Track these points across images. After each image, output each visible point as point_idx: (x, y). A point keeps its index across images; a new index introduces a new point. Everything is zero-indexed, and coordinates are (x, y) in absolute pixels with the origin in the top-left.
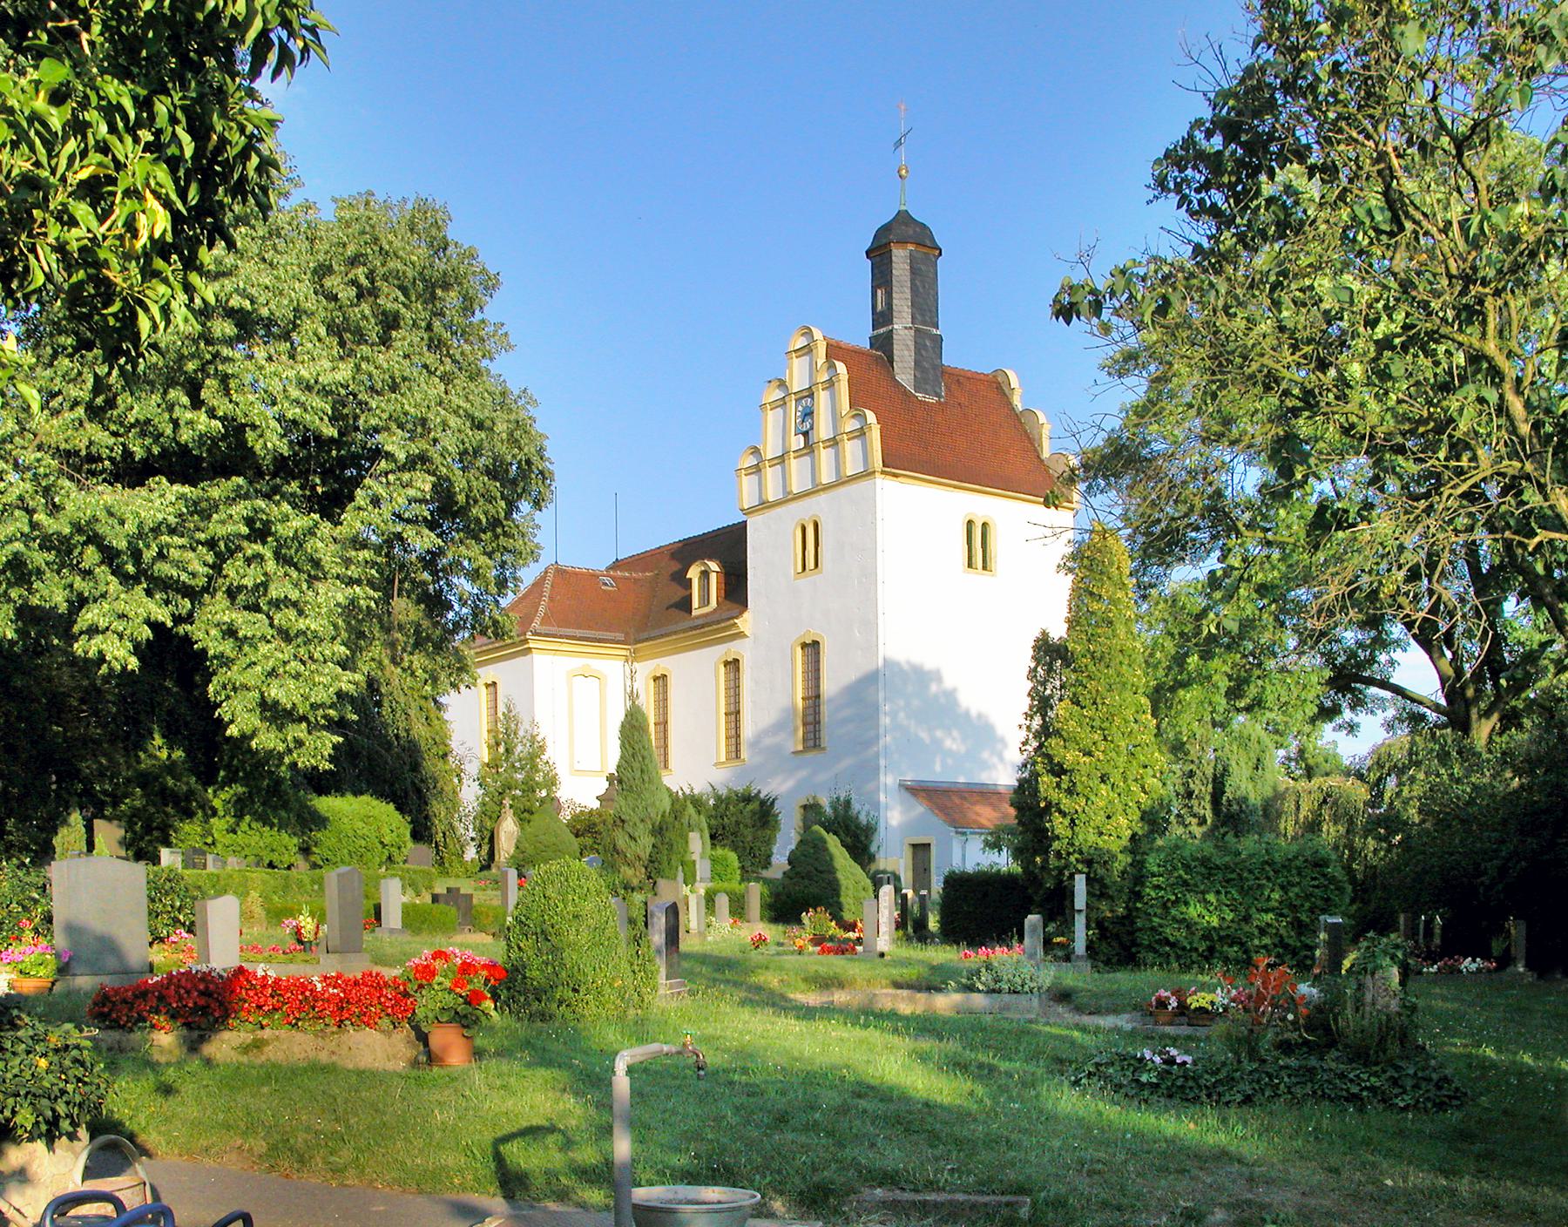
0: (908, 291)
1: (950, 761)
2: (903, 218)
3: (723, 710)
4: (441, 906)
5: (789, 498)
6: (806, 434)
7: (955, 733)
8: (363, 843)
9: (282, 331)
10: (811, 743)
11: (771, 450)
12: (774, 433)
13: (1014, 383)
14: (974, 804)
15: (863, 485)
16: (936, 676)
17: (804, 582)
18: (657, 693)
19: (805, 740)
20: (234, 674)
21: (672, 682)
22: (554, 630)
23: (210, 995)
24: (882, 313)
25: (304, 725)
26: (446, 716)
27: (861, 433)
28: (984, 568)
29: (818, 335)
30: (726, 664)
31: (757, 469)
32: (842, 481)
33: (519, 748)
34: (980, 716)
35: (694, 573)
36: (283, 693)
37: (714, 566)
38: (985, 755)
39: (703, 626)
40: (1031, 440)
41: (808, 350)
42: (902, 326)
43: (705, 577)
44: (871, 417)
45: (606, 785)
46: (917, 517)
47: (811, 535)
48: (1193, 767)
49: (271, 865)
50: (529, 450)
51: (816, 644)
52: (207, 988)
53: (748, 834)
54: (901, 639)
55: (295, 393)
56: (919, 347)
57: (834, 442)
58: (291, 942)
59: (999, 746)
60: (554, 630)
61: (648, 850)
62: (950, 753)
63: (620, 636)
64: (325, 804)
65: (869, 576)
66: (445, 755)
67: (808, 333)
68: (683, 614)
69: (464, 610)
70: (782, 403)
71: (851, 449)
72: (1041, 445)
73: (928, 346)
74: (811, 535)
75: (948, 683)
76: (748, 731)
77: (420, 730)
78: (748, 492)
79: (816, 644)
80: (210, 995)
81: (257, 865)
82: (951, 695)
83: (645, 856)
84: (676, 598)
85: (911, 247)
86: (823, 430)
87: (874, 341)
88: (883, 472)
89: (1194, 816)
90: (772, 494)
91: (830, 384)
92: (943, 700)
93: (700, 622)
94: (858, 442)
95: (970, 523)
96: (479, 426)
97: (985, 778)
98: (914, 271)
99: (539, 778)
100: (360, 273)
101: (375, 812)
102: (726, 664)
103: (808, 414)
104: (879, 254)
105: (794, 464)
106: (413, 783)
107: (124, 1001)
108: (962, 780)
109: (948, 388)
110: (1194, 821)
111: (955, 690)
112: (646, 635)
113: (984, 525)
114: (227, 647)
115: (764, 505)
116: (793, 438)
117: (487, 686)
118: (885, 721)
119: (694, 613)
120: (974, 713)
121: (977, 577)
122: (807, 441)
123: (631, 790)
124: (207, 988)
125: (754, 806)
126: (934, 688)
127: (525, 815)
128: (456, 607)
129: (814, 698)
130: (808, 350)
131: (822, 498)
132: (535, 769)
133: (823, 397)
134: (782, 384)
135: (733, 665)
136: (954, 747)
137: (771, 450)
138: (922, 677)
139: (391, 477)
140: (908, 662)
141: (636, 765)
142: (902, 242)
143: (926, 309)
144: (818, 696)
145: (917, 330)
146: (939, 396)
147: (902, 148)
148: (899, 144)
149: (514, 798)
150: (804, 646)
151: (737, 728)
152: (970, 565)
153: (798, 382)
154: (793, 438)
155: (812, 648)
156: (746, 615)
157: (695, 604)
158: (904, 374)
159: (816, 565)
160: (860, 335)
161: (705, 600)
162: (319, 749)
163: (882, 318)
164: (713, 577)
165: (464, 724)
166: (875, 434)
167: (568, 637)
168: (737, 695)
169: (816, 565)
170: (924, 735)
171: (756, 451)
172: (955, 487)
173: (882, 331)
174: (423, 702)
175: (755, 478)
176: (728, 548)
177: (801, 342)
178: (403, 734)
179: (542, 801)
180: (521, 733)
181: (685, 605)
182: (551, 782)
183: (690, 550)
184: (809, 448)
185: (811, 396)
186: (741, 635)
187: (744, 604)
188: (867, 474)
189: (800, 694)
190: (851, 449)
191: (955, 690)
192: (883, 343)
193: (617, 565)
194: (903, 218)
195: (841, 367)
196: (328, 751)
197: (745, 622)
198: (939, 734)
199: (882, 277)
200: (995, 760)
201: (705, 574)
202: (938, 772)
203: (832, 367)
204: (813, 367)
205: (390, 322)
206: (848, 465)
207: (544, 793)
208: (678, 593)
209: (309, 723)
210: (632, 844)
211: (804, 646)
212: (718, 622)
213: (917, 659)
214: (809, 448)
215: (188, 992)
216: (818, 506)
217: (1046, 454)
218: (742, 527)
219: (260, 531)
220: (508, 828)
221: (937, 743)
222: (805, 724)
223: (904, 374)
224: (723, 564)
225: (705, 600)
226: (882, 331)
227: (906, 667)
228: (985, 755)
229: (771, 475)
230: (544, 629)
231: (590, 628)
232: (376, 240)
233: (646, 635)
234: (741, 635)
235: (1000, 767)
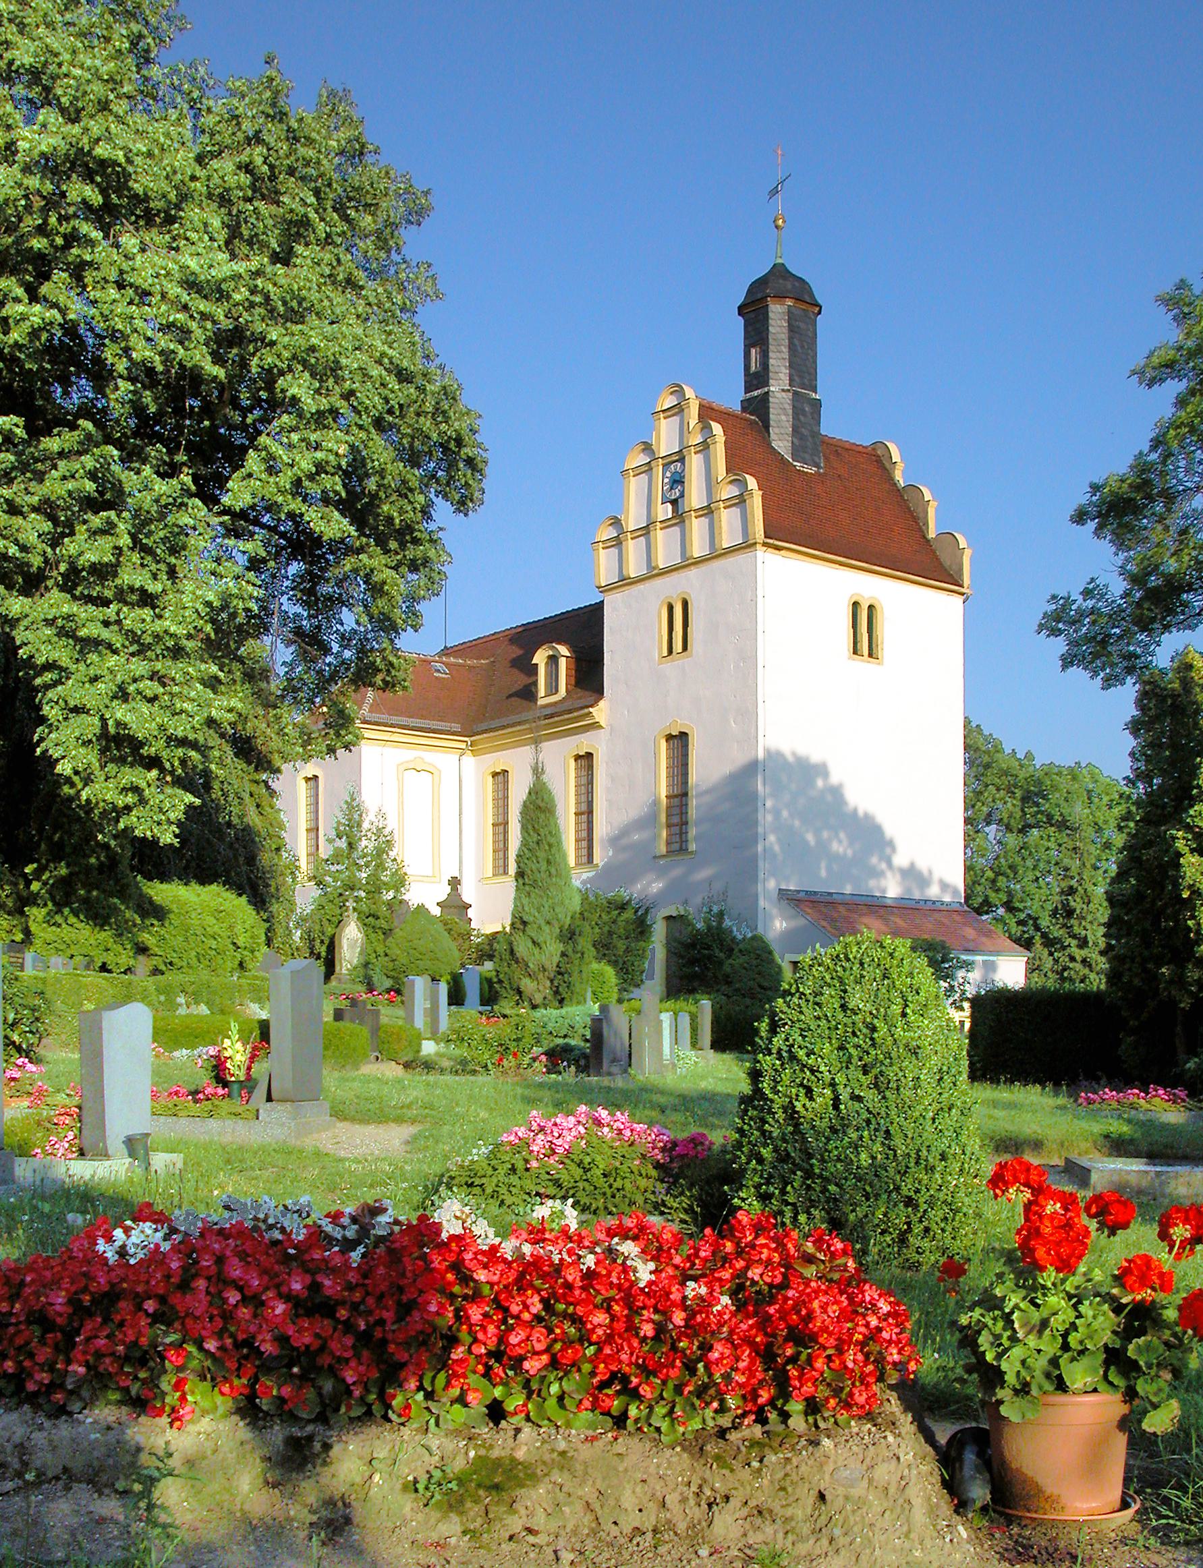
0: (785, 350)
1: (835, 867)
2: (779, 272)
3: (572, 810)
4: (345, 1025)
5: (654, 573)
6: (674, 502)
7: (842, 835)
8: (214, 944)
9: (158, 216)
10: (676, 846)
11: (634, 519)
12: (636, 501)
13: (896, 457)
14: (862, 915)
15: (741, 558)
16: (821, 770)
17: (671, 668)
18: (496, 791)
19: (668, 843)
20: (72, 691)
21: (512, 777)
22: (384, 718)
23: (326, 1308)
24: (755, 373)
25: (154, 773)
26: (278, 803)
27: (740, 501)
28: (870, 655)
29: (689, 393)
30: (578, 758)
31: (618, 542)
32: (716, 554)
33: (364, 843)
34: (866, 816)
35: (540, 658)
36: (138, 719)
37: (563, 650)
38: (874, 860)
39: (552, 716)
40: (915, 519)
41: (678, 410)
42: (779, 387)
43: (553, 665)
44: (752, 483)
45: (448, 889)
46: (802, 594)
47: (679, 617)
48: (1073, 883)
49: (104, 968)
50: (459, 425)
51: (683, 736)
52: (315, 1287)
53: (621, 945)
54: (782, 730)
55: (174, 290)
56: (797, 412)
57: (708, 511)
58: (204, 1078)
59: (888, 850)
60: (384, 718)
61: (556, 959)
62: (836, 858)
63: (456, 727)
64: (161, 892)
65: (748, 661)
66: (278, 849)
67: (679, 391)
68: (524, 703)
69: (347, 654)
70: (648, 468)
71: (728, 519)
72: (926, 524)
73: (807, 411)
74: (679, 617)
75: (834, 779)
76: (602, 828)
77: (253, 819)
78: (605, 566)
79: (683, 736)
80: (326, 1308)
81: (87, 967)
82: (836, 792)
83: (551, 965)
84: (517, 687)
85: (790, 303)
86: (695, 497)
87: (747, 405)
88: (765, 544)
89: (1074, 937)
90: (634, 569)
91: (705, 447)
92: (829, 798)
93: (548, 711)
94: (736, 511)
95: (856, 605)
96: (404, 376)
97: (873, 887)
98: (792, 329)
99: (385, 877)
100: (257, 155)
101: (227, 906)
102: (578, 758)
103: (678, 481)
104: (753, 313)
105: (659, 535)
106: (249, 878)
107: (42, 1319)
108: (848, 890)
109: (826, 458)
110: (1074, 942)
111: (912, 865)
112: (484, 726)
113: (871, 607)
114: (62, 654)
115: (624, 581)
116: (660, 508)
117: (307, 779)
118: (766, 819)
119: (540, 702)
120: (861, 813)
121: (862, 666)
122: (675, 510)
123: (534, 885)
124: (315, 1287)
125: (628, 915)
126: (820, 783)
127: (369, 919)
128: (335, 647)
129: (680, 796)
130: (678, 410)
131: (693, 572)
132: (381, 866)
133: (695, 463)
134: (647, 448)
135: (585, 760)
136: (841, 850)
137: (634, 519)
138: (807, 772)
139: (295, 437)
140: (794, 754)
141: (541, 855)
142: (780, 297)
143: (804, 371)
144: (685, 794)
145: (795, 393)
146: (818, 466)
147: (779, 196)
148: (774, 192)
149: (357, 900)
150: (670, 738)
151: (590, 830)
152: (855, 652)
153: (666, 444)
154: (660, 508)
155: (679, 741)
156: (602, 703)
157: (542, 692)
158: (781, 443)
159: (685, 648)
160: (732, 397)
161: (553, 688)
162: (161, 815)
163: (757, 379)
164: (563, 663)
165: (296, 812)
166: (756, 502)
167: (403, 727)
168: (590, 792)
169: (685, 648)
170: (810, 838)
171: (616, 522)
172: (841, 564)
173: (756, 393)
174: (254, 788)
175: (615, 551)
176: (582, 632)
177: (669, 401)
178: (235, 820)
179: (389, 905)
180: (366, 825)
181: (528, 693)
182: (400, 882)
183: (531, 636)
184: (679, 517)
185: (682, 460)
186: (596, 726)
187: (599, 691)
188: (747, 545)
189: (663, 792)
190: (728, 519)
191: (912, 865)
192: (758, 408)
193: (446, 651)
194: (779, 272)
195: (717, 428)
196: (177, 814)
197: (601, 712)
198: (825, 834)
199: (756, 334)
200: (884, 866)
201: (553, 660)
202: (822, 879)
203: (706, 428)
204: (683, 430)
205: (296, 229)
206: (724, 536)
207: (391, 894)
208: (522, 680)
209: (162, 769)
210: (536, 951)
211: (670, 738)
212: (570, 711)
213: (802, 751)
214: (679, 517)
215: (253, 1300)
216: (690, 583)
217: (932, 534)
218: (596, 611)
219: (107, 497)
220: (352, 937)
221: (822, 846)
222: (669, 826)
223: (781, 443)
224: (573, 648)
225: (553, 688)
226: (756, 393)
227: (790, 759)
228: (874, 860)
229: (634, 548)
230: (375, 717)
231: (423, 717)
232: (282, 116)
233: (484, 726)
234: (596, 726)
235: (889, 874)
